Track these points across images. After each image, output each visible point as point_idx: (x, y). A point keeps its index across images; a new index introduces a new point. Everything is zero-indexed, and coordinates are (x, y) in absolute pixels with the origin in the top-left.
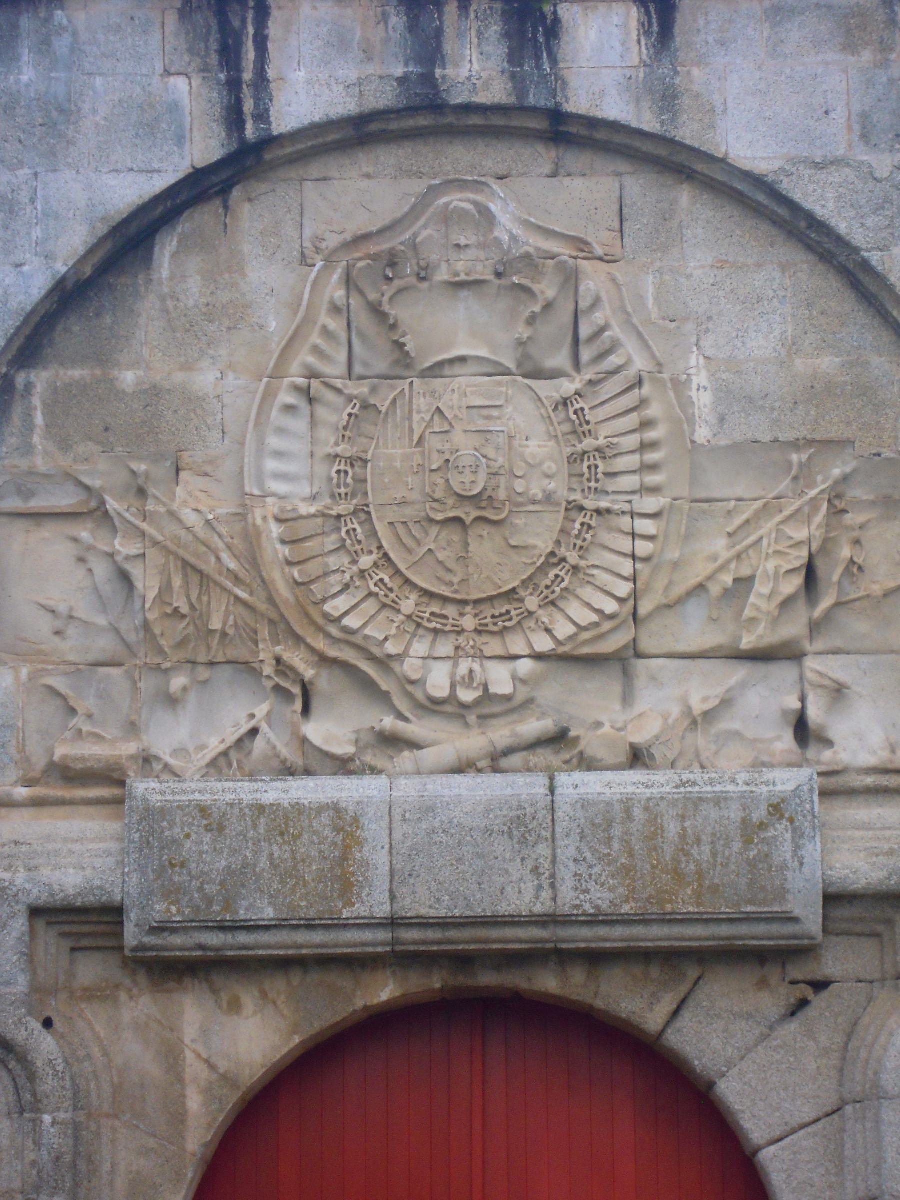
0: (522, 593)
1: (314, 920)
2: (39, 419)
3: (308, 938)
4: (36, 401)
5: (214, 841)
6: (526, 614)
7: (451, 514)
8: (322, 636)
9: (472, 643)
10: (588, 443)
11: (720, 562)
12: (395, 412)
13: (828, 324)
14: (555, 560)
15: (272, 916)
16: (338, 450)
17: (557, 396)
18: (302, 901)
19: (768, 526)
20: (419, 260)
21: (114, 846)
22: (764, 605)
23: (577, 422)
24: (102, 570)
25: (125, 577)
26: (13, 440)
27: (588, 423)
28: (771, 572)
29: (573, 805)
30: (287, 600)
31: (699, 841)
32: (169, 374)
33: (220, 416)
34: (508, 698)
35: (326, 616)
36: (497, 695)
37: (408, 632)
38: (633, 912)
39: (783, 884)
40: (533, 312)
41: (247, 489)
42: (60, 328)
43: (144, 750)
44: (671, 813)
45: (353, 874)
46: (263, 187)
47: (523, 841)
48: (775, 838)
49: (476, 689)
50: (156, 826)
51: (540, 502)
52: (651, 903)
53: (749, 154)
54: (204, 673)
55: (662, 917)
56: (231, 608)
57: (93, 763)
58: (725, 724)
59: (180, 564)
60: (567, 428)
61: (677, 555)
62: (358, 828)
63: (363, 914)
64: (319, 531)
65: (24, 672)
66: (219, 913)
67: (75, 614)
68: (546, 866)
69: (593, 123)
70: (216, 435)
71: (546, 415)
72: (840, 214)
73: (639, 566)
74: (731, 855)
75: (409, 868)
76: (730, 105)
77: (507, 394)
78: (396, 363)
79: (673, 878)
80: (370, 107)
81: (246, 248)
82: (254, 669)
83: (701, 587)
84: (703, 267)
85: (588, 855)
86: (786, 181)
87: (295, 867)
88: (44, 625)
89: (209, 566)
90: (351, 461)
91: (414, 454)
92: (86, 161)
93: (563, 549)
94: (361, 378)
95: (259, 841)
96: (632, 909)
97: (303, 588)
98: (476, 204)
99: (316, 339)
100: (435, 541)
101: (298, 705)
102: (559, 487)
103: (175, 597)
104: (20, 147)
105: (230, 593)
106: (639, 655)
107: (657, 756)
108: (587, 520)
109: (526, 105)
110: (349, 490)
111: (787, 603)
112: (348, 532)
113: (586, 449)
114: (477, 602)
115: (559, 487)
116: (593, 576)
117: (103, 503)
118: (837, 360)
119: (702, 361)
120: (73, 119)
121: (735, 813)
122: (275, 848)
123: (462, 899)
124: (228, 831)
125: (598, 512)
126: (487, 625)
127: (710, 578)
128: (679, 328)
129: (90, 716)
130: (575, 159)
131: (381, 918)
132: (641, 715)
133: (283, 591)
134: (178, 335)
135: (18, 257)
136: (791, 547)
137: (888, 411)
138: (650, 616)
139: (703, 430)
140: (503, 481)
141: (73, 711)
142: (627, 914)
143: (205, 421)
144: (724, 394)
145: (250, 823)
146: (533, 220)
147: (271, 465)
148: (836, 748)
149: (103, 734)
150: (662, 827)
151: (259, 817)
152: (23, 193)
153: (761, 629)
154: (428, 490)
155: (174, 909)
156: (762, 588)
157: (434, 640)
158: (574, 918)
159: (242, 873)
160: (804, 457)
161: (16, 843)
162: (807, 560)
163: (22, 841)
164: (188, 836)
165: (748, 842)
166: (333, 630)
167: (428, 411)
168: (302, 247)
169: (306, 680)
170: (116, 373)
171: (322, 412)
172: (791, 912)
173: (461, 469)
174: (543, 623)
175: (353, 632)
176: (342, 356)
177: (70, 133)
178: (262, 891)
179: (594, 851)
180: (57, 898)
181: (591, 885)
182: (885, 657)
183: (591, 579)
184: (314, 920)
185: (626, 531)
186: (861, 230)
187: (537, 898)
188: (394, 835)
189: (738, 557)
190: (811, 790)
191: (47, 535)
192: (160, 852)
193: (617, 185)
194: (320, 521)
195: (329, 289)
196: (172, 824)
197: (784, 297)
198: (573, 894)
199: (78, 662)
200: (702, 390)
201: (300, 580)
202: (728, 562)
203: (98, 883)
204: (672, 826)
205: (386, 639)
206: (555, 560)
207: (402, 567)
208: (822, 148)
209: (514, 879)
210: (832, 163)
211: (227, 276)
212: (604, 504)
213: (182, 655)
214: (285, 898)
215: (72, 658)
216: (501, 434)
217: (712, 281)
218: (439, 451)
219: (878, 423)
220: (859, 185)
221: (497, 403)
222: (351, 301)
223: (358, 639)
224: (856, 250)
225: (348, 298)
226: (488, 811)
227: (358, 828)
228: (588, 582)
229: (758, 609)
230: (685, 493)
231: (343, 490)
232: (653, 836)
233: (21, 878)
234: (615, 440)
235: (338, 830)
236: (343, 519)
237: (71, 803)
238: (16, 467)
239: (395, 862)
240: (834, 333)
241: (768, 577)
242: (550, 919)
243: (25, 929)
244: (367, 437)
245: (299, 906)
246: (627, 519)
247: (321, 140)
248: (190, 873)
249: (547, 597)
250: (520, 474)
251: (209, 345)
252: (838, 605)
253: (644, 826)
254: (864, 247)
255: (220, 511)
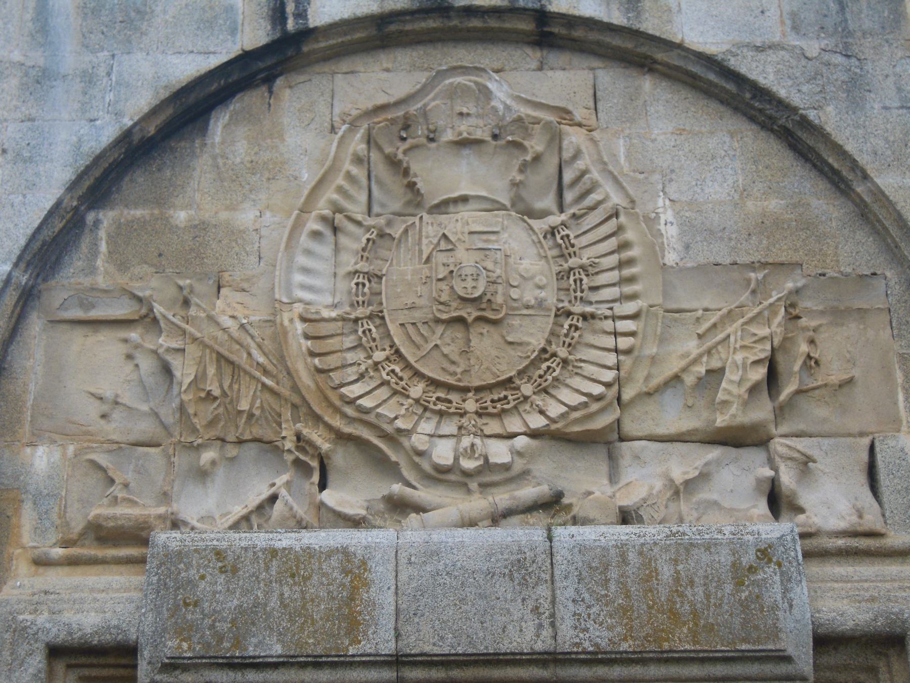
0: (518, 382)
1: (321, 656)
2: (103, 247)
3: (315, 677)
4: (102, 234)
5: (228, 582)
6: (522, 399)
7: (455, 314)
8: (338, 417)
9: (473, 422)
10: (573, 262)
11: (692, 357)
12: (407, 240)
13: (772, 176)
14: (547, 356)
15: (280, 652)
16: (358, 267)
17: (546, 227)
18: (309, 638)
19: (732, 328)
20: (428, 124)
21: (136, 595)
22: (735, 390)
23: (563, 245)
24: (147, 364)
25: (167, 370)
26: (80, 263)
27: (573, 246)
28: (739, 362)
29: (570, 550)
30: (309, 386)
31: (692, 583)
32: (216, 213)
33: (257, 245)
34: (506, 467)
35: (342, 397)
36: (496, 465)
37: (416, 414)
38: (631, 650)
39: (775, 624)
40: (525, 160)
41: (277, 296)
42: (127, 179)
43: (172, 514)
44: (664, 557)
45: (360, 613)
46: (302, 78)
47: (524, 583)
48: (764, 580)
49: (476, 459)
50: (173, 568)
51: (532, 307)
52: (649, 641)
53: (701, 40)
54: (232, 451)
55: (660, 655)
56: (258, 393)
57: (123, 522)
58: (704, 495)
59: (214, 355)
60: (555, 252)
61: (655, 350)
62: (365, 570)
63: (369, 651)
64: (339, 332)
65: (71, 449)
66: (229, 650)
67: (119, 400)
68: (546, 606)
69: (572, 21)
70: (254, 259)
71: (536, 240)
72: (779, 84)
73: (622, 358)
74: (723, 596)
75: (414, 607)
76: (683, 6)
77: (503, 223)
78: (408, 203)
79: (669, 618)
80: (390, 8)
81: (286, 121)
82: (277, 447)
83: (677, 378)
84: (665, 134)
85: (586, 596)
86: (732, 59)
87: (304, 607)
88: (93, 409)
89: (241, 359)
90: (370, 276)
91: (422, 268)
92: (155, 47)
93: (554, 346)
94: (378, 215)
95: (271, 582)
96: (630, 646)
97: (322, 375)
98: (476, 83)
99: (340, 181)
100: (440, 338)
101: (316, 478)
102: (550, 297)
103: (208, 382)
104: (102, 37)
105: (258, 380)
106: (622, 439)
107: (645, 517)
108: (574, 322)
109: (517, 6)
110: (366, 298)
111: (754, 390)
112: (364, 332)
113: (572, 266)
114: (478, 389)
115: (550, 297)
116: (581, 367)
117: (151, 310)
118: (782, 202)
119: (667, 202)
120: (147, 17)
121: (725, 557)
122: (286, 589)
123: (464, 637)
124: (241, 573)
125: (585, 317)
126: (486, 408)
127: (684, 370)
128: (646, 178)
129: (126, 486)
130: (555, 58)
131: (385, 655)
132: (627, 484)
133: (305, 379)
134: (226, 184)
135: (93, 114)
136: (755, 342)
137: (829, 241)
138: (632, 401)
139: (671, 255)
140: (500, 289)
141: (112, 481)
142: (626, 652)
143: (245, 249)
144: (687, 227)
145: (262, 565)
146: (523, 95)
147: (298, 278)
148: (807, 514)
149: (135, 499)
150: (656, 570)
151: (271, 560)
152: (101, 69)
153: (733, 410)
154: (435, 295)
155: (185, 645)
156: (732, 375)
157: (439, 423)
158: (573, 656)
159: (252, 612)
160: (760, 276)
161: (46, 593)
162: (769, 353)
163: (51, 591)
164: (203, 577)
165: (739, 584)
166: (349, 411)
167: (435, 236)
168: (332, 120)
169: (323, 452)
170: (172, 212)
171: (343, 240)
172: (784, 651)
173: (463, 277)
174: (537, 406)
175: (367, 411)
176: (363, 198)
177: (144, 27)
178: (271, 629)
179: (592, 592)
180: (75, 636)
181: (590, 624)
182: (843, 439)
183: (579, 371)
184: (321, 656)
185: (609, 330)
186: (798, 95)
187: (538, 636)
188: (399, 577)
189: (709, 352)
190: (794, 540)
191: (102, 338)
192: (175, 591)
193: (591, 76)
194: (340, 324)
195: (353, 145)
196: (188, 566)
197: (734, 156)
198: (572, 632)
199: (120, 440)
200: (669, 225)
201: (320, 367)
202: (701, 356)
203: (115, 622)
204: (665, 569)
205: (396, 418)
206: (547, 356)
207: (412, 360)
208: (761, 36)
209: (515, 618)
210: (770, 47)
211: (269, 141)
212: (589, 309)
213: (213, 433)
214: (294, 635)
215: (114, 437)
216: (498, 252)
217: (672, 144)
218: (444, 265)
219: (821, 250)
220: (794, 62)
221: (495, 229)
222: (371, 154)
223: (371, 418)
224: (795, 110)
225: (369, 152)
226: (490, 555)
227: (365, 570)
228: (577, 374)
229: (729, 393)
230: (659, 300)
231: (360, 299)
232: (648, 579)
233: (42, 619)
234: (597, 260)
235: (346, 572)
236: (360, 322)
237: (103, 562)
238: (80, 284)
239: (400, 602)
240: (778, 183)
241: (737, 367)
242: (550, 657)
243: (43, 665)
244: (382, 260)
245: (307, 643)
246: (610, 322)
247: (349, 38)
248: (203, 611)
249: (540, 385)
250: (515, 284)
251: (251, 191)
252: (799, 392)
253: (639, 569)
254: (802, 106)
255: (252, 318)
